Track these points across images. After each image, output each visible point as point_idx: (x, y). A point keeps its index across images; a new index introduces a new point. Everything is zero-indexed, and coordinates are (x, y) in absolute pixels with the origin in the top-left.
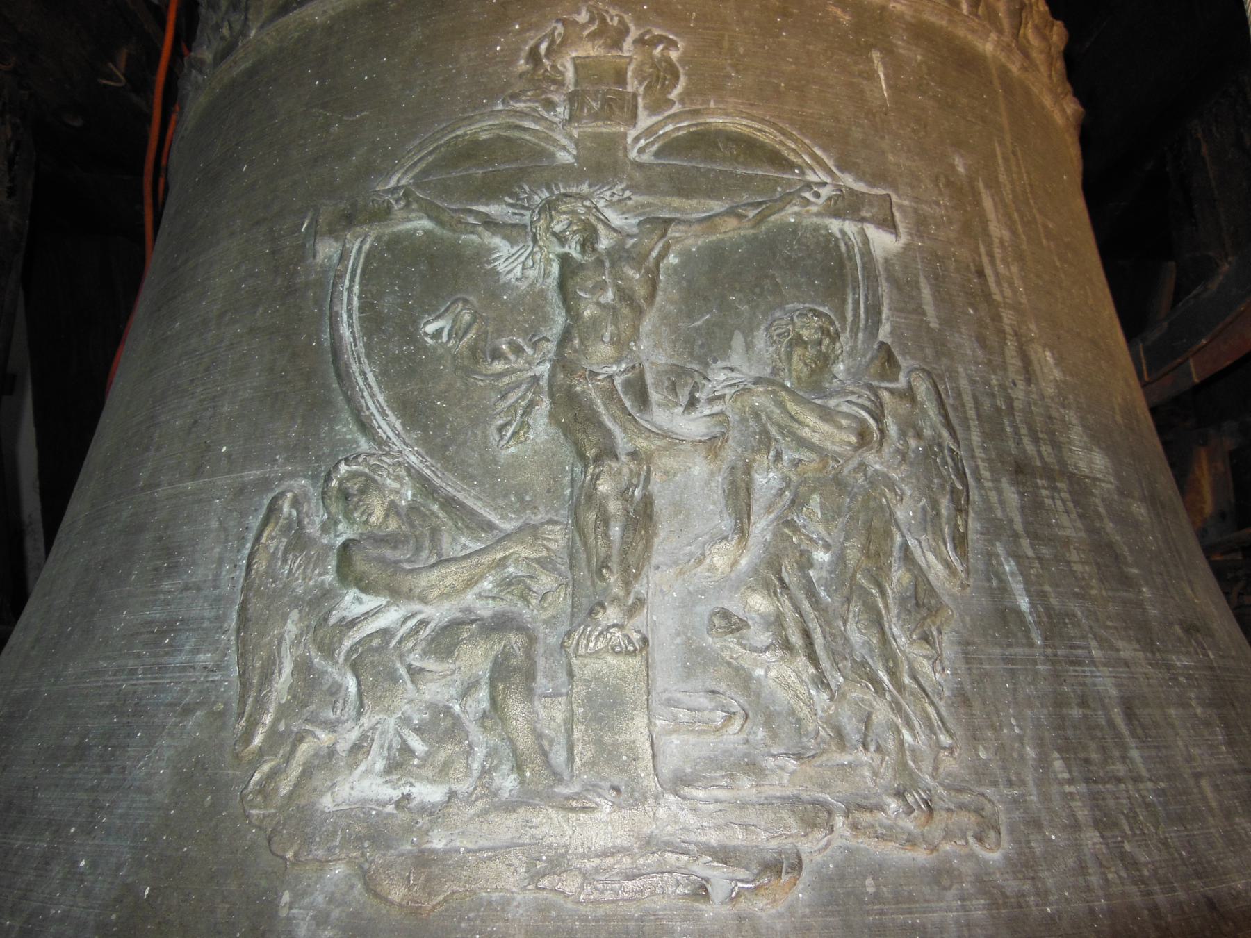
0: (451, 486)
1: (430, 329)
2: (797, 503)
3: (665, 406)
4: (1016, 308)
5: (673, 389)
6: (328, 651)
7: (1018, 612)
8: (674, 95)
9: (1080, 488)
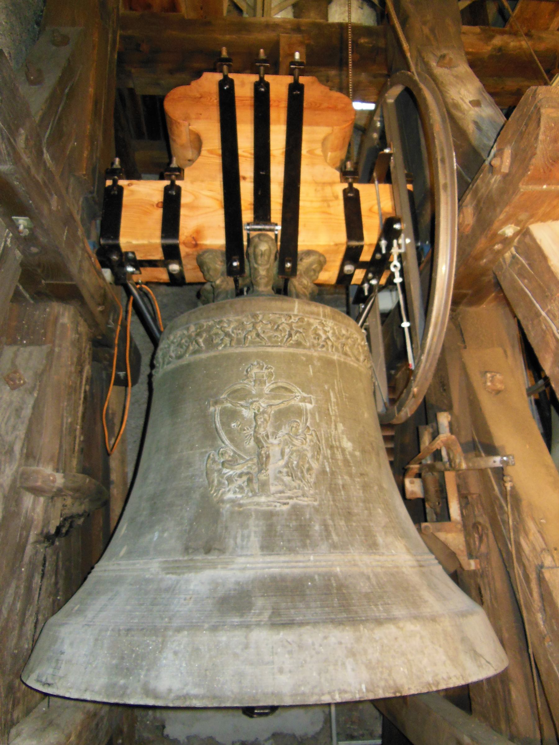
0: (239, 453)
1: (233, 425)
2: (292, 454)
3: (272, 438)
4: (336, 416)
5: (273, 435)
6: (222, 478)
7: (327, 471)
8: (272, 379)
9: (343, 450)
